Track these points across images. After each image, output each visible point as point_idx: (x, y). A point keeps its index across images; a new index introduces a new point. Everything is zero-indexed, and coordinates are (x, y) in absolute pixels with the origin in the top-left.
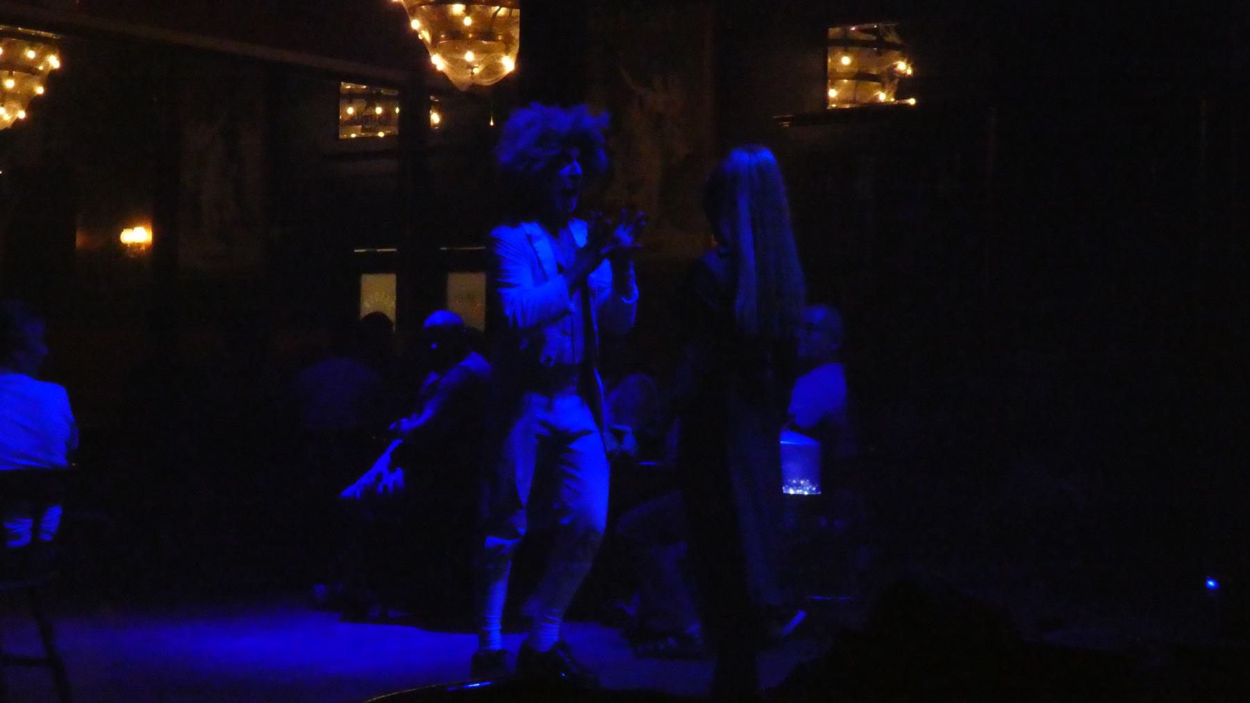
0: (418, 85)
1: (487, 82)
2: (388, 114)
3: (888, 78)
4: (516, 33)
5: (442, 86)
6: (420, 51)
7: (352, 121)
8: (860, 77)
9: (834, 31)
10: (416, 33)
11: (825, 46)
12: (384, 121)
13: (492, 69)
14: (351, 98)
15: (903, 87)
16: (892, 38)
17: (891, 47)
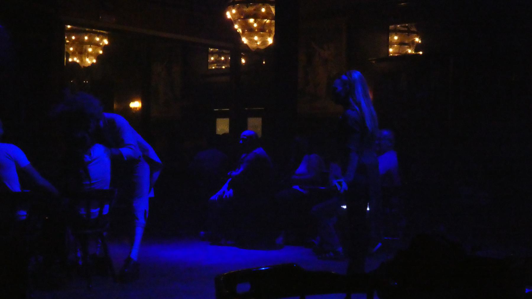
0: (238, 49)
1: (262, 47)
2: (226, 59)
3: (412, 44)
4: (273, 29)
5: (246, 50)
6: (238, 36)
7: (213, 63)
8: (401, 44)
9: (391, 27)
10: (236, 30)
11: (388, 33)
12: (224, 63)
13: (264, 42)
14: (212, 54)
15: (418, 47)
16: (414, 29)
17: (413, 32)
